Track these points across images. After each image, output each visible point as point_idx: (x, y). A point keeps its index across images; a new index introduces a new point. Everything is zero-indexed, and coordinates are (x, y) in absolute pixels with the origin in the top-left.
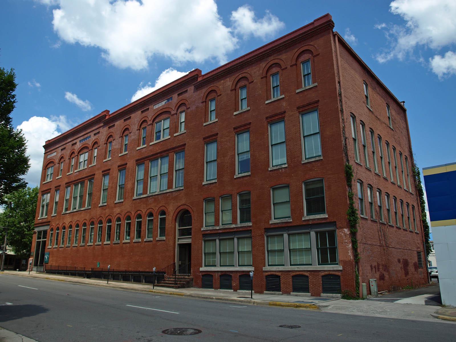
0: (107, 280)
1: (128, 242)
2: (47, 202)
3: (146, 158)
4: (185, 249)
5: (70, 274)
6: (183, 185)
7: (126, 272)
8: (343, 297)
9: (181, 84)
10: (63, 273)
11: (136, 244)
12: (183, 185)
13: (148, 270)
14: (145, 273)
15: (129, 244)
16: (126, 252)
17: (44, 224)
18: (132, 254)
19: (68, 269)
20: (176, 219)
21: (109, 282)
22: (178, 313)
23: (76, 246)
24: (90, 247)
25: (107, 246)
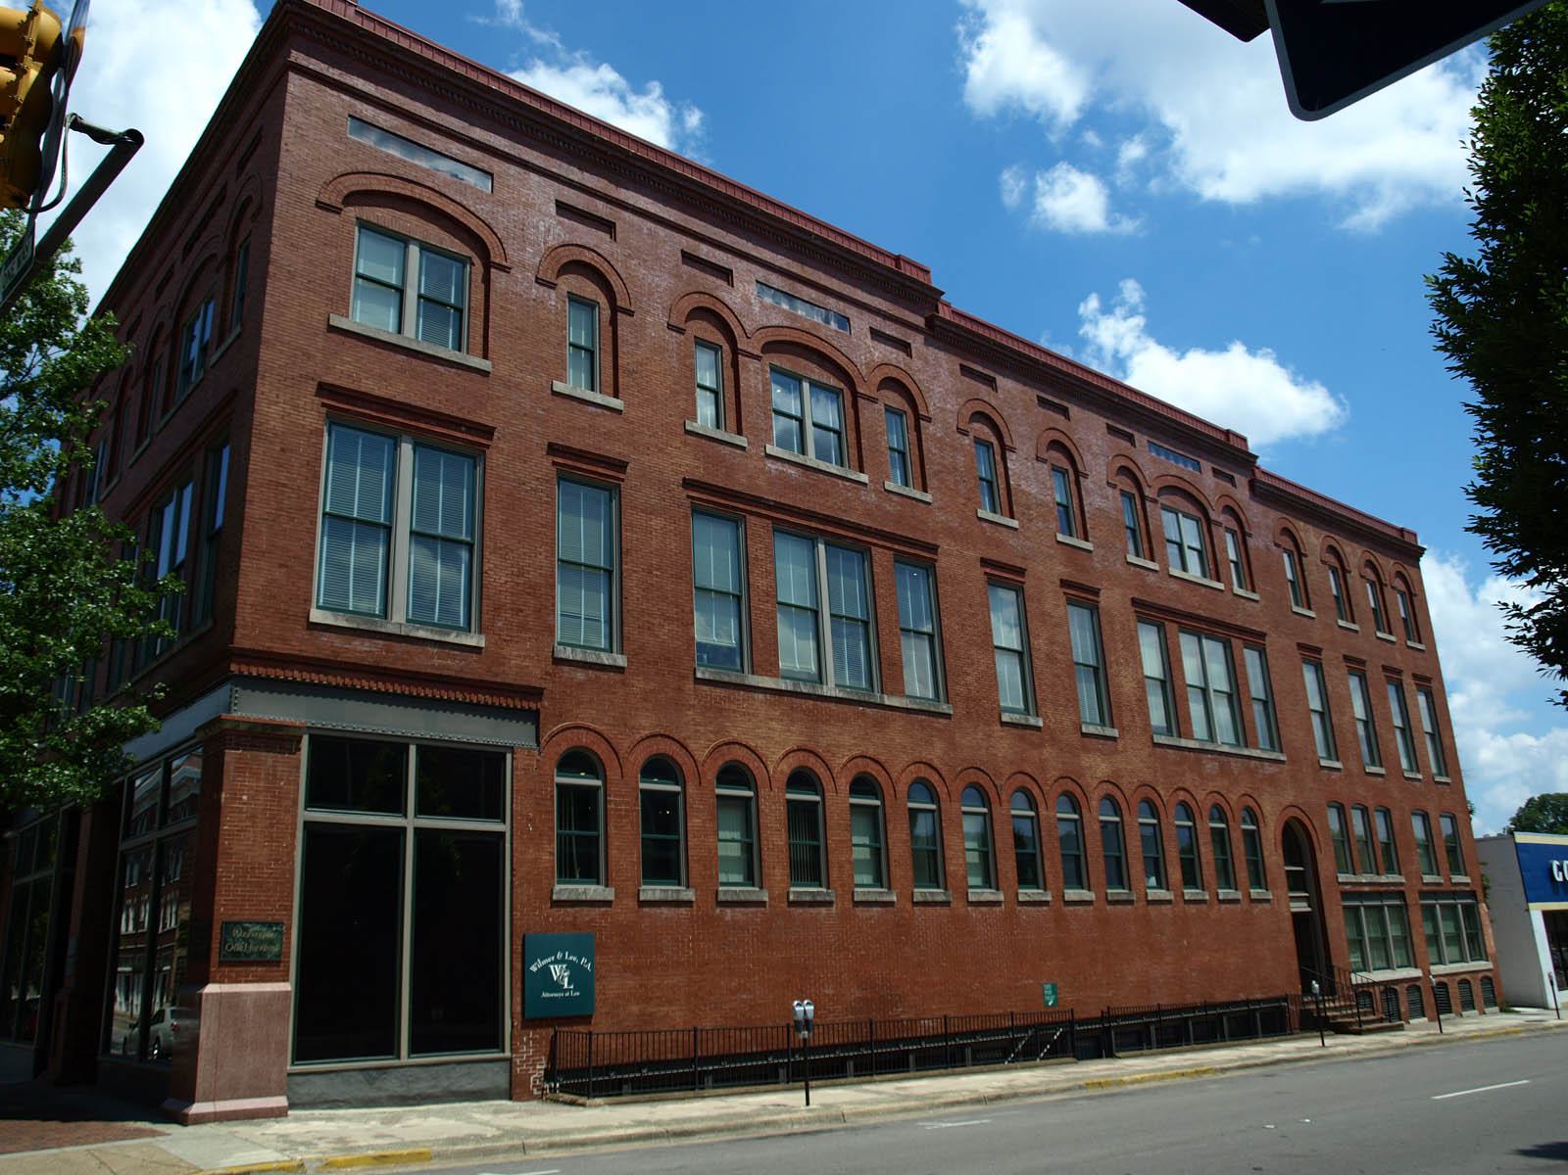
0: (803, 1084)
1: (1168, 898)
2: (205, 340)
3: (432, 681)
4: (1308, 932)
5: (851, 1065)
6: (121, 956)
7: (1206, 1006)
8: (1502, 1011)
9: (757, 219)
10: (709, 1080)
11: (1193, 909)
12: (121, 956)
13: (1242, 996)
14: (982, 1037)
15: (1169, 906)
16: (1164, 938)
17: (281, 674)
18: (1185, 943)
19: (951, 1030)
20: (883, 902)
21: (1447, 1029)
22: (1525, 1082)
23: (886, 898)
24: (984, 909)
25: (1081, 909)
